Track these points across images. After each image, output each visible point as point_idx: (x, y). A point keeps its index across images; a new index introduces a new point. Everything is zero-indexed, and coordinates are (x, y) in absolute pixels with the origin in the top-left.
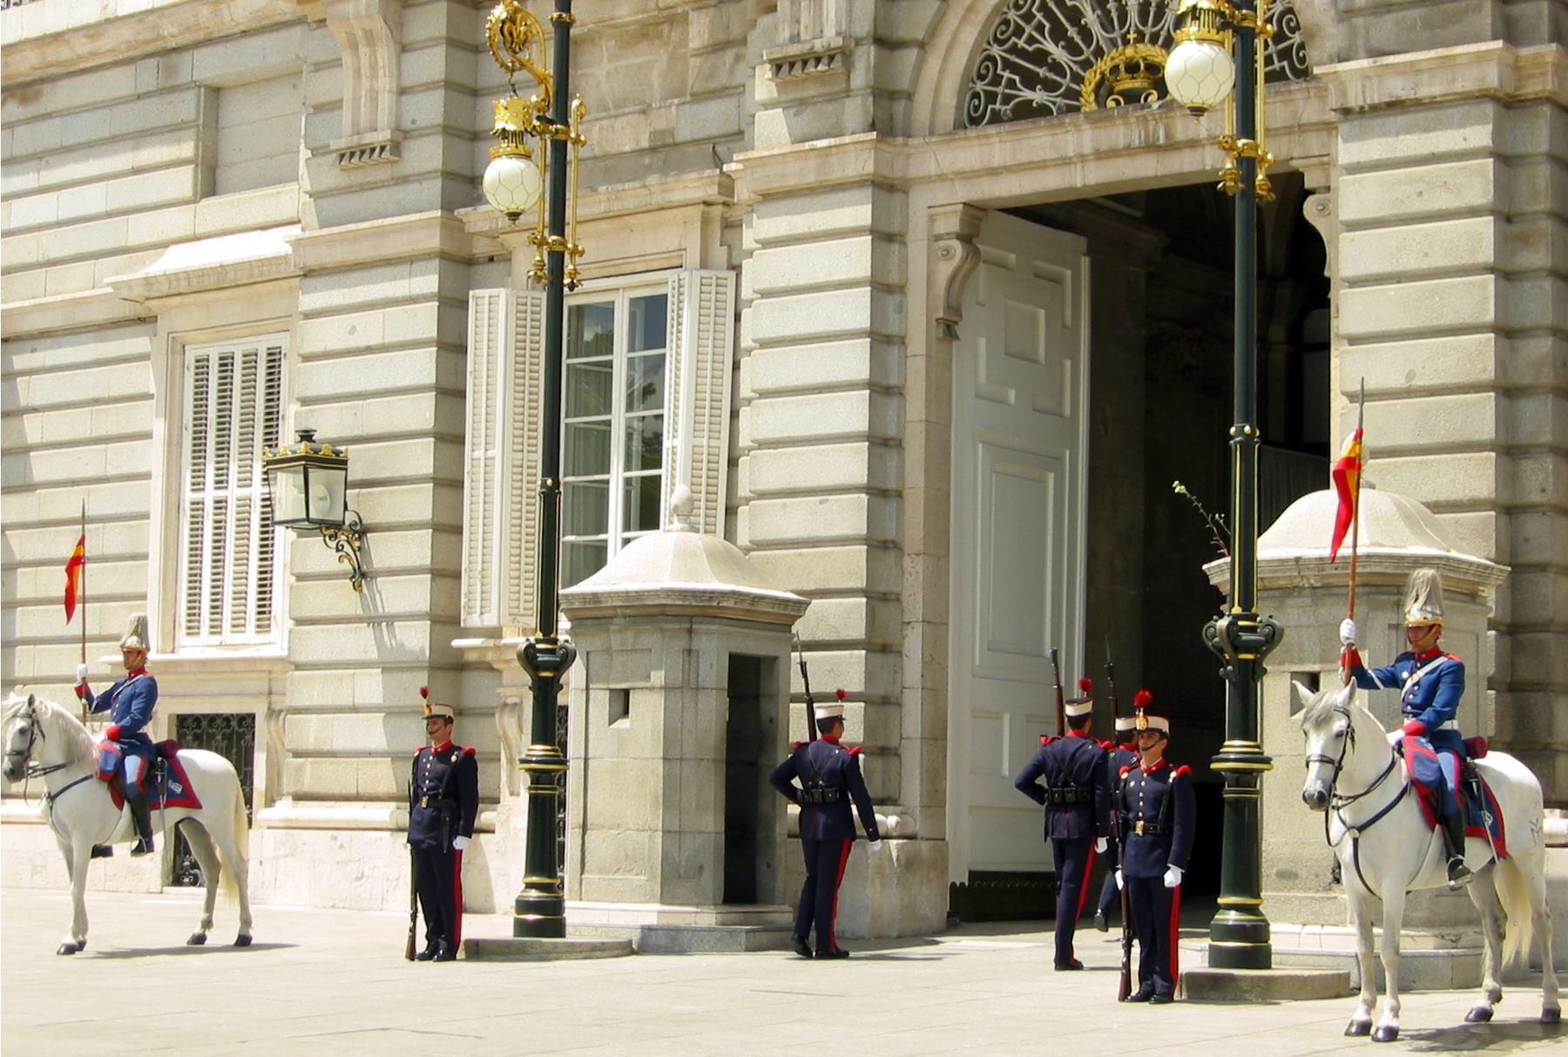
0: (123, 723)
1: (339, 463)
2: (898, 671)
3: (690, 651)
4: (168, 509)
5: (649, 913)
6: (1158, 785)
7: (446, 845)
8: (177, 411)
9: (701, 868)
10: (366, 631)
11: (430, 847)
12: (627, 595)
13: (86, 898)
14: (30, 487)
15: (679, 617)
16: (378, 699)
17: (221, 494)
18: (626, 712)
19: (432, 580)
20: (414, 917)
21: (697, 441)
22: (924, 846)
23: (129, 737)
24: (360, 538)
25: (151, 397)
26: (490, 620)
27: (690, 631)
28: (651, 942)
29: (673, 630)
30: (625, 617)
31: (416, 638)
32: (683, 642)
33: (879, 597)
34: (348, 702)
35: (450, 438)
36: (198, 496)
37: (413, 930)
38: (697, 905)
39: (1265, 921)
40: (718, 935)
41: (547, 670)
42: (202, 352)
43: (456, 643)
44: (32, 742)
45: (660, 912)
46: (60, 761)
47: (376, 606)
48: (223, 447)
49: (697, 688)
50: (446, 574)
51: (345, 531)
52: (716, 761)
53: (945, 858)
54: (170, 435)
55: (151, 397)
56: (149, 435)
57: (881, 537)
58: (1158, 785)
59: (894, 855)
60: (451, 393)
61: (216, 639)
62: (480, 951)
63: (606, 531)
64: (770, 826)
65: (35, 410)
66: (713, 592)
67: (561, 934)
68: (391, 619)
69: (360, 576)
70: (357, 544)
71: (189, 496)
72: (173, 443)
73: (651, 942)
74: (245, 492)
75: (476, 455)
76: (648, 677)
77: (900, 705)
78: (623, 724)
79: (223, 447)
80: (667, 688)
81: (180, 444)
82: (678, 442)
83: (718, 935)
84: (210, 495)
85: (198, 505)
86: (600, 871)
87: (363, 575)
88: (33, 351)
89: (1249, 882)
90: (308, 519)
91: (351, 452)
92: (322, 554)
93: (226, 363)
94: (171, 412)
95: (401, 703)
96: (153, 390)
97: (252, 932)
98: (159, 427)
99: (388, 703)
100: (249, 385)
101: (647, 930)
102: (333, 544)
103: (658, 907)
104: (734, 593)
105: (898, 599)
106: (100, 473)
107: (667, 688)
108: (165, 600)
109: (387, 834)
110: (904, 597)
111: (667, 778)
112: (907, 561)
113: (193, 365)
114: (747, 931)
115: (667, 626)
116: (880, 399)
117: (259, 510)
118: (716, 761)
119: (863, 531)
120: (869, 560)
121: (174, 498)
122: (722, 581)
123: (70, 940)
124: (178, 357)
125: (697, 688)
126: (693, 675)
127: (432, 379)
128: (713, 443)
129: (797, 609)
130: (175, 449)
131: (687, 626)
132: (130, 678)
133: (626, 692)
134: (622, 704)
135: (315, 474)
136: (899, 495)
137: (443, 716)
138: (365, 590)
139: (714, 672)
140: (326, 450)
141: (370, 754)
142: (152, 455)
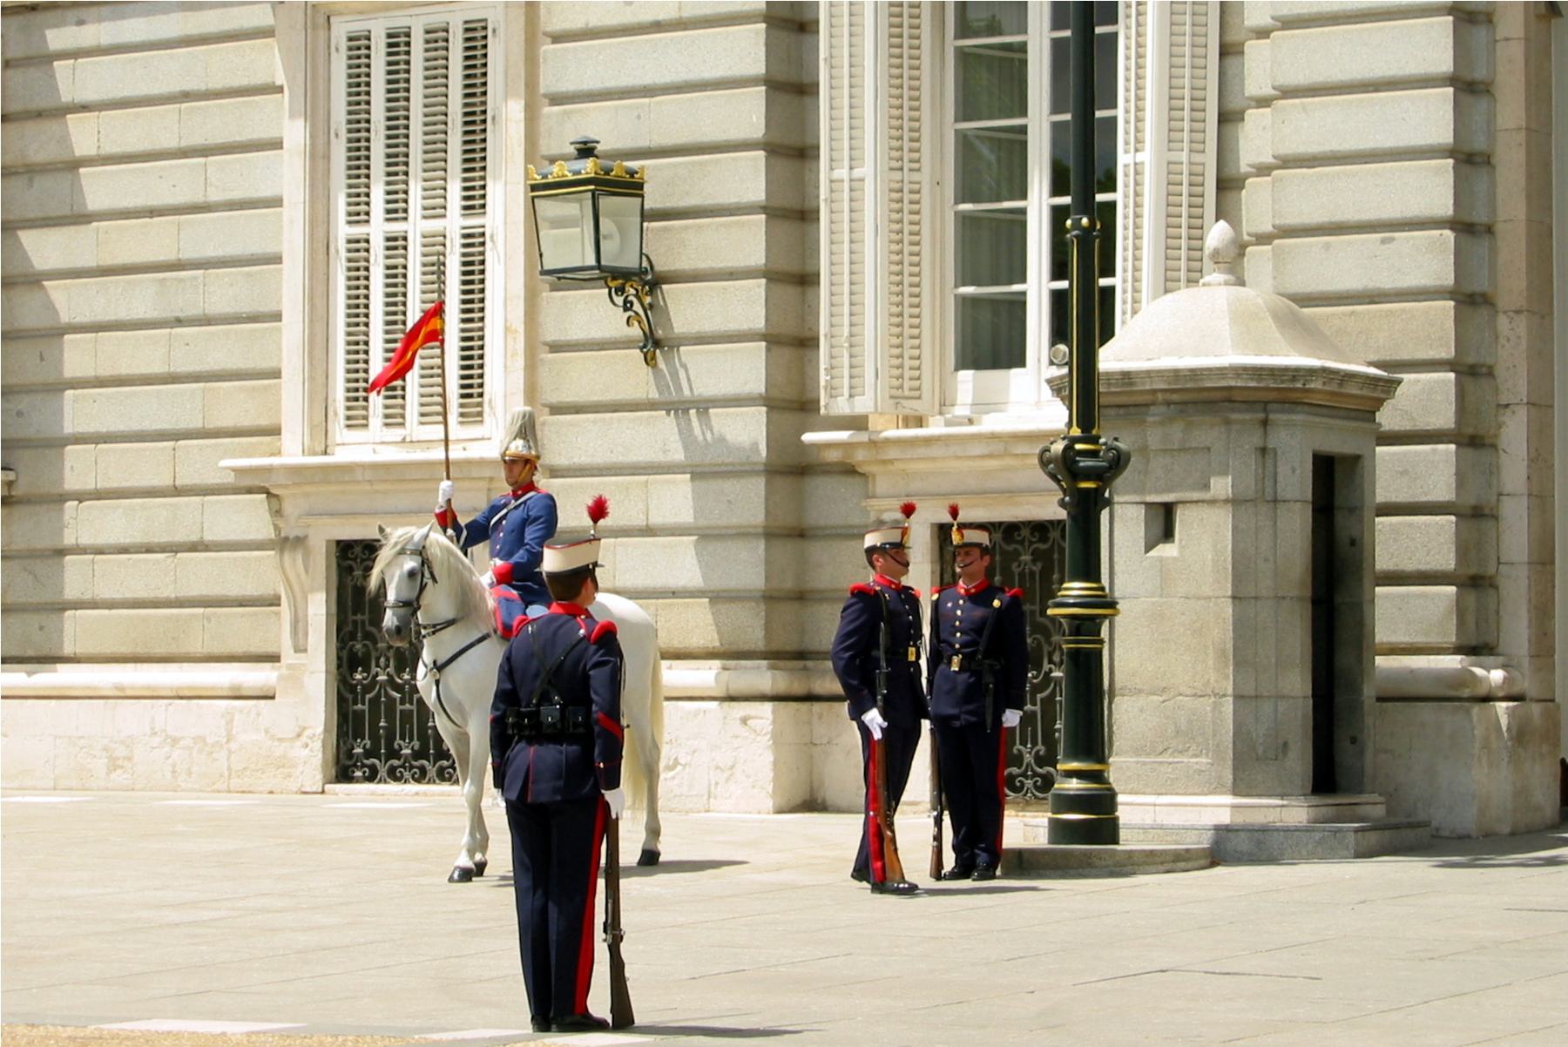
0: (516, 558)
1: (631, 186)
2: (1493, 471)
3: (1263, 451)
4: (313, 251)
5: (1217, 808)
6: (979, 612)
7: (989, 720)
8: (321, 112)
9: (1285, 744)
10: (665, 423)
11: (970, 725)
12: (1176, 374)
13: (483, 804)
14: (85, 218)
15: (1250, 404)
16: (686, 516)
17: (396, 228)
18: (1168, 534)
19: (768, 350)
20: (938, 822)
21: (1174, 156)
22: (1536, 709)
23: (523, 578)
24: (651, 292)
25: (280, 89)
26: (863, 405)
27: (1265, 423)
28: (1223, 849)
29: (1243, 422)
30: (1168, 404)
31: (747, 430)
32: (1256, 439)
33: (1470, 372)
34: (639, 521)
35: (792, 151)
36: (358, 231)
37: (938, 838)
38: (1282, 796)
39: (1111, 789)
40: (1318, 836)
41: (1088, 479)
42: (358, 26)
43: (808, 437)
44: (422, 588)
45: (1234, 807)
46: (450, 615)
47: (679, 388)
48: (397, 161)
49: (1275, 501)
50: (793, 342)
51: (637, 284)
52: (1300, 599)
53: (1556, 725)
54: (313, 145)
55: (280, 89)
56: (277, 144)
57: (1469, 289)
58: (979, 612)
59: (1504, 721)
60: (791, 88)
61: (396, 434)
62: (1027, 864)
63: (1023, 280)
64: (1355, 687)
65: (85, 108)
66: (1297, 370)
67: (1117, 843)
68: (704, 406)
69: (654, 344)
70: (648, 300)
71: (343, 231)
72: (318, 157)
73: (1223, 849)
74: (435, 225)
75: (837, 174)
76: (1206, 487)
77: (1495, 518)
78: (1166, 550)
79: (397, 161)
80: (1236, 502)
81: (327, 157)
82: (1145, 157)
83: (1318, 836)
84: (378, 229)
85: (359, 245)
86: (1137, 751)
87: (657, 344)
88: (80, 23)
89: (1091, 738)
90: (599, 266)
91: (648, 168)
92: (595, 313)
93: (398, 42)
94: (314, 110)
95: (723, 522)
96: (280, 80)
97: (661, 847)
98: (295, 133)
99: (703, 522)
100: (437, 73)
101: (1222, 831)
102: (619, 300)
103: (1229, 799)
104: (1324, 370)
105: (1490, 373)
106: (198, 198)
107: (1236, 502)
108: (312, 379)
109: (714, 704)
110: (1500, 372)
111: (1239, 624)
112: (1503, 322)
113: (344, 44)
114: (1357, 831)
115: (1234, 416)
116: (1467, 99)
117: (459, 250)
118: (1300, 599)
119: (1449, 280)
120: (1458, 320)
121: (321, 234)
122: (1301, 354)
123: (465, 861)
124: (322, 34)
125: (1275, 501)
126: (1269, 483)
127: (759, 68)
128: (1197, 158)
129: (1388, 387)
130: (321, 164)
131: (1261, 416)
132: (517, 497)
133: (1168, 510)
134: (1163, 523)
135: (606, 202)
136: (1489, 230)
137: (979, 545)
138: (661, 364)
139: (1297, 481)
140: (619, 168)
141: (674, 594)
142: (287, 174)
